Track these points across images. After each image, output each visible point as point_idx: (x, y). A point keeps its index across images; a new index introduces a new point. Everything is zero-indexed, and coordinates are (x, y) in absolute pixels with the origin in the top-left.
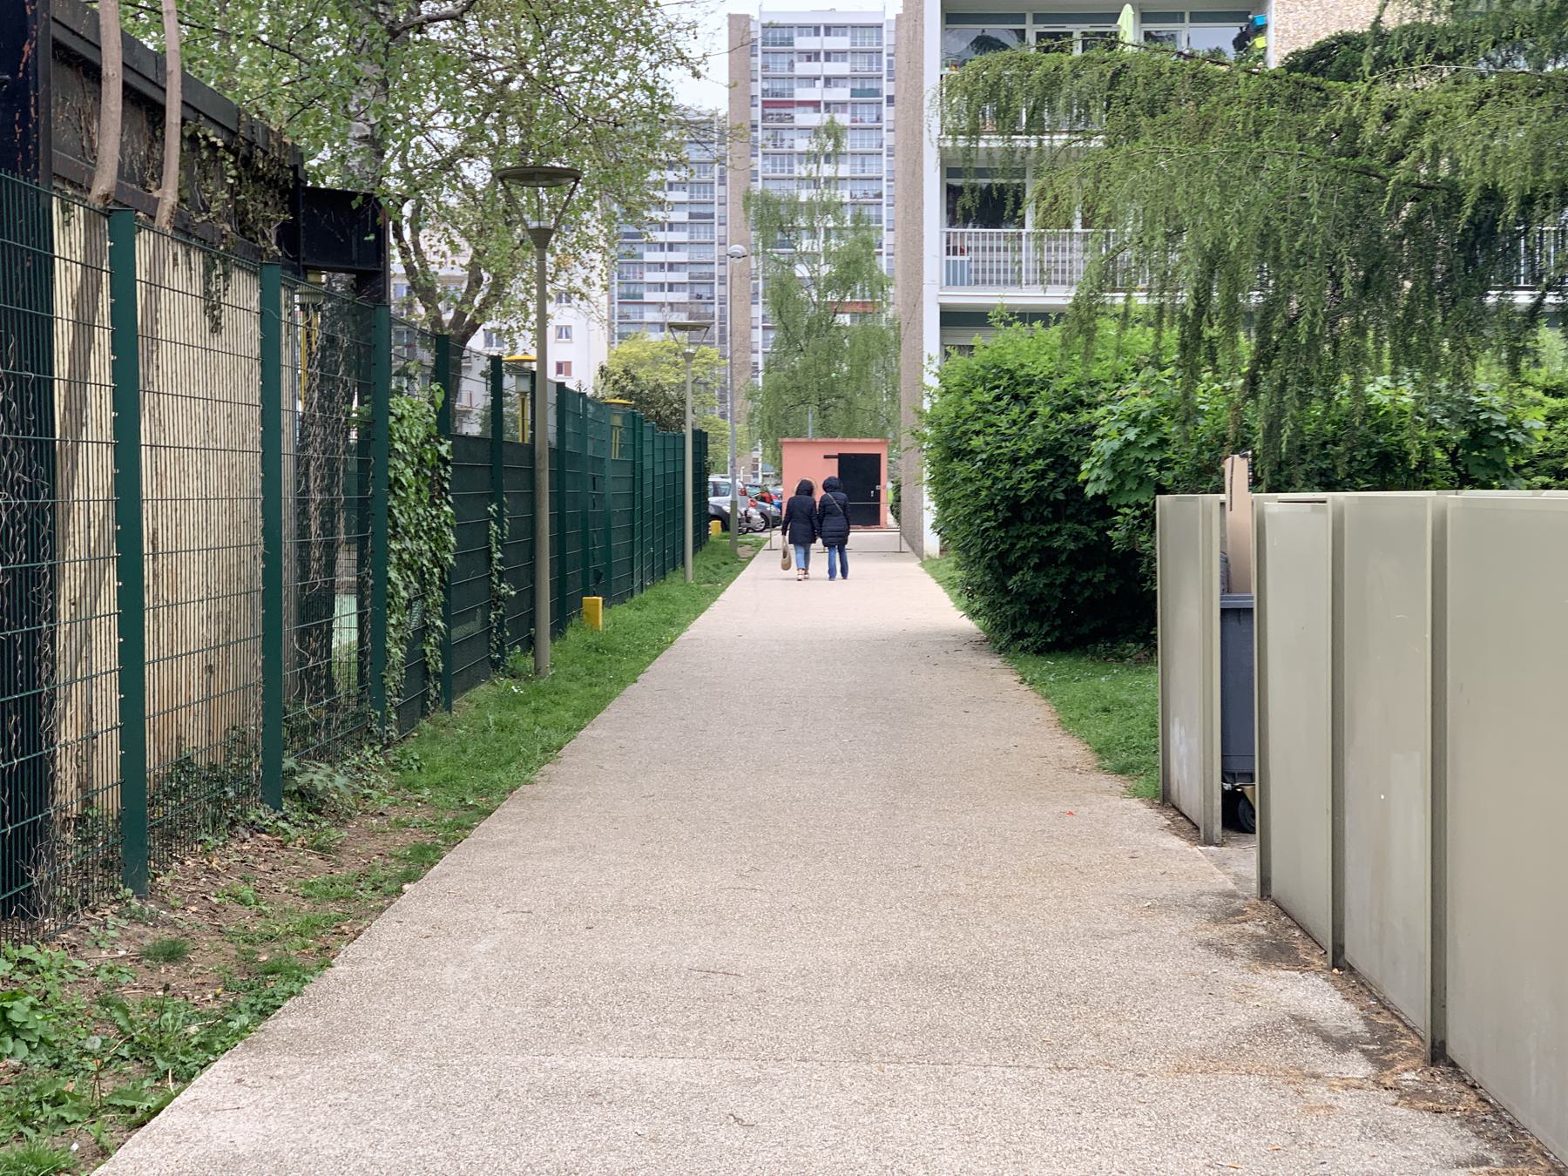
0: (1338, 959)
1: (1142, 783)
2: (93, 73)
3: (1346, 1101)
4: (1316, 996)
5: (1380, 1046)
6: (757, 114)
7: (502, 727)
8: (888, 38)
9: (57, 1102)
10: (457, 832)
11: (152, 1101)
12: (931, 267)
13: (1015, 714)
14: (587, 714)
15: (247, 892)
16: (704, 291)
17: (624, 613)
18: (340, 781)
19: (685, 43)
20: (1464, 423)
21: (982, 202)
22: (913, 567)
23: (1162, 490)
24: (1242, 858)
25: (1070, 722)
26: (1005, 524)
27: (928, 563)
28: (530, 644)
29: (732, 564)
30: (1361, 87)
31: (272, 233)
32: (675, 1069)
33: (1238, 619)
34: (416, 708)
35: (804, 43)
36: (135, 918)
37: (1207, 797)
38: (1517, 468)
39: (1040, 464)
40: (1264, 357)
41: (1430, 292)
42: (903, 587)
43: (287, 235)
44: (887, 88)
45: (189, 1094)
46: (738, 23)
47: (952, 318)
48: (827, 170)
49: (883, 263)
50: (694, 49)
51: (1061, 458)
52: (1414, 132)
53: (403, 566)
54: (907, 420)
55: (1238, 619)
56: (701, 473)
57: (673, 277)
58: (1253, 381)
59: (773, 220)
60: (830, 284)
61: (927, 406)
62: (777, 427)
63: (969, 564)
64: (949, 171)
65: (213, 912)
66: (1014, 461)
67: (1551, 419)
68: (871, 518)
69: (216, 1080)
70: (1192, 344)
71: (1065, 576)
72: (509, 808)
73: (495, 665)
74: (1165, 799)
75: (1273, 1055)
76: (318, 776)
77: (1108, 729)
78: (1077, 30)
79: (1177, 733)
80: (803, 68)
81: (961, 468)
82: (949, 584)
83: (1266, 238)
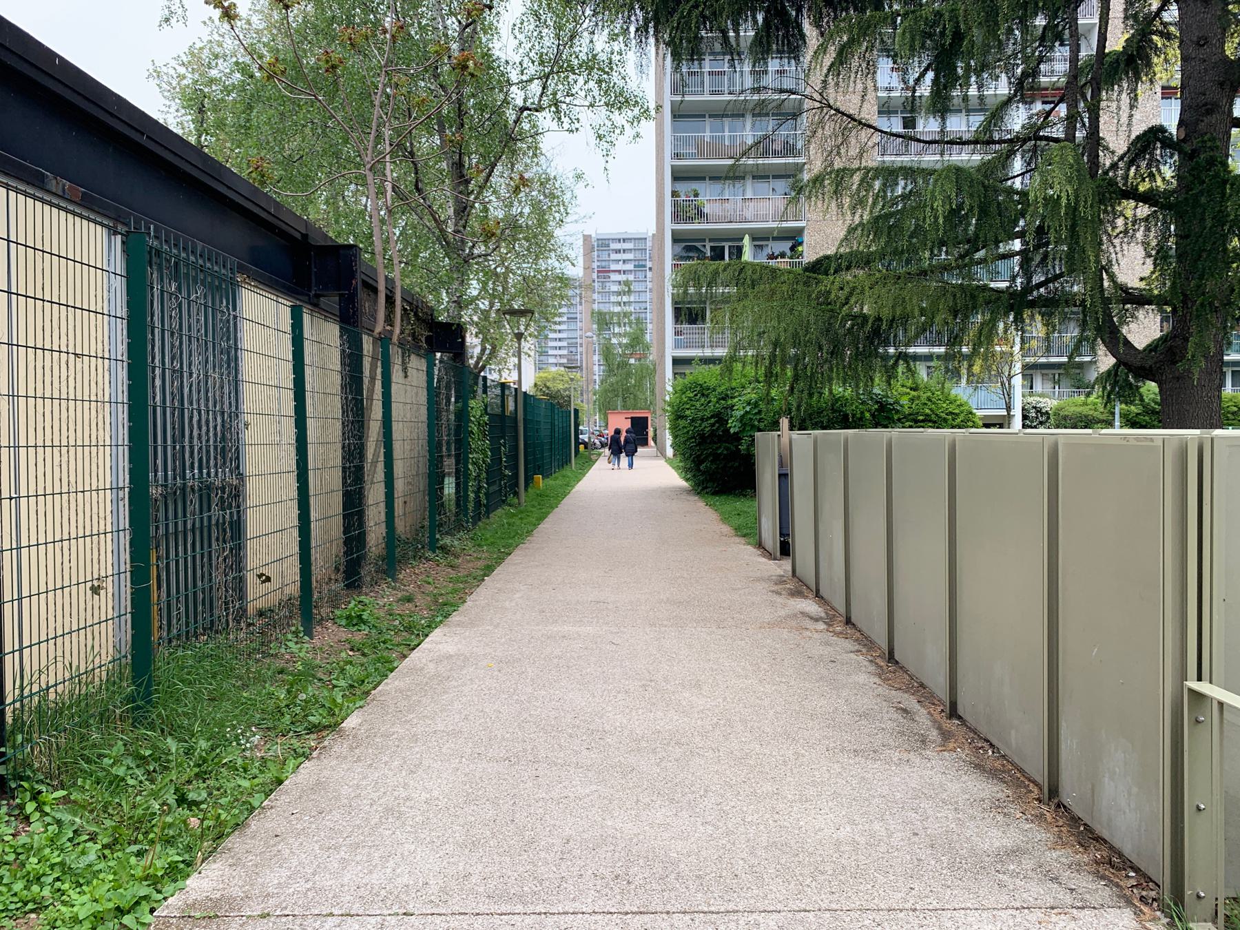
0: (818, 594)
1: (751, 540)
2: (375, 290)
3: (816, 635)
4: (810, 606)
5: (829, 621)
6: (595, 276)
7: (509, 524)
8: (649, 244)
9: (384, 642)
10: (500, 560)
11: (415, 643)
12: (667, 342)
13: (704, 516)
14: (541, 519)
15: (430, 580)
16: (573, 349)
17: (550, 482)
18: (456, 543)
19: (566, 251)
20: (877, 402)
21: (688, 314)
22: (662, 462)
23: (760, 430)
24: (786, 564)
25: (725, 519)
26: (699, 444)
27: (668, 460)
28: (516, 494)
29: (589, 463)
30: (831, 278)
31: (423, 339)
32: (590, 629)
33: (784, 477)
34: (477, 518)
35: (614, 246)
36: (394, 589)
37: (774, 543)
38: (899, 420)
39: (713, 420)
40: (796, 378)
41: (857, 355)
42: (658, 470)
43: (428, 340)
44: (649, 264)
45: (427, 640)
46: (587, 238)
47: (677, 362)
48: (625, 299)
49: (648, 337)
50: (572, 255)
51: (721, 418)
52: (851, 294)
53: (474, 463)
54: (659, 404)
55: (784, 477)
56: (577, 425)
57: (560, 344)
58: (792, 388)
59: (603, 321)
60: (626, 346)
61: (667, 398)
62: (606, 407)
63: (685, 460)
64: (675, 302)
65: (419, 587)
66: (702, 419)
67: (912, 400)
68: (645, 443)
69: (436, 634)
70: (769, 374)
71: (721, 464)
72: (517, 552)
73: (504, 501)
74: (760, 545)
75: (794, 623)
76: (447, 541)
77: (741, 520)
78: (727, 245)
79: (764, 520)
80: (614, 256)
81: (682, 423)
82: (676, 468)
83: (795, 335)
